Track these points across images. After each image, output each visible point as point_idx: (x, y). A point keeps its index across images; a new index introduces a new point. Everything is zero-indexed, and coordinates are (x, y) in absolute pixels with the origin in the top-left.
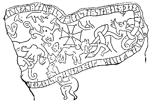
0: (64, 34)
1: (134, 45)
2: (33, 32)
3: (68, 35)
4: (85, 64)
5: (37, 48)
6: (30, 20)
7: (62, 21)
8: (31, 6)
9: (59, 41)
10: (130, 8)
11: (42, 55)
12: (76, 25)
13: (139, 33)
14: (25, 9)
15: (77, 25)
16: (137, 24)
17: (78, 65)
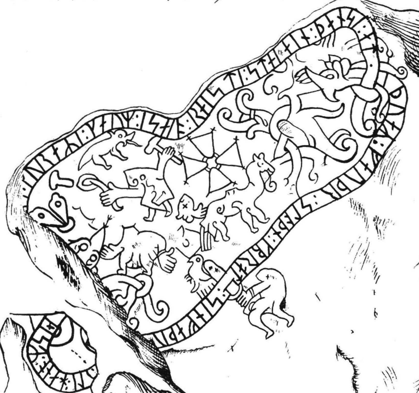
0: (193, 167)
1: (385, 112)
2: (113, 195)
3: (205, 165)
4: (279, 221)
5: (139, 233)
6: (90, 168)
7: (174, 134)
8: (79, 132)
9: (186, 189)
10: (337, 24)
11: (162, 247)
12: (213, 129)
13: (382, 76)
14: (69, 145)
15: (218, 127)
16: (370, 55)
17: (263, 228)
